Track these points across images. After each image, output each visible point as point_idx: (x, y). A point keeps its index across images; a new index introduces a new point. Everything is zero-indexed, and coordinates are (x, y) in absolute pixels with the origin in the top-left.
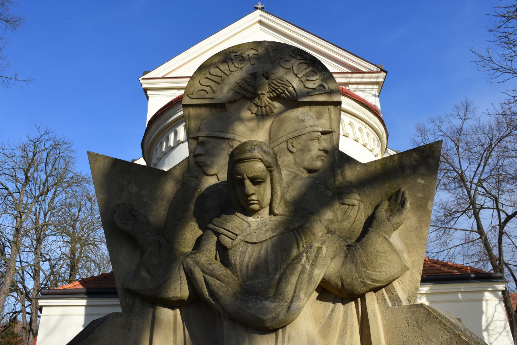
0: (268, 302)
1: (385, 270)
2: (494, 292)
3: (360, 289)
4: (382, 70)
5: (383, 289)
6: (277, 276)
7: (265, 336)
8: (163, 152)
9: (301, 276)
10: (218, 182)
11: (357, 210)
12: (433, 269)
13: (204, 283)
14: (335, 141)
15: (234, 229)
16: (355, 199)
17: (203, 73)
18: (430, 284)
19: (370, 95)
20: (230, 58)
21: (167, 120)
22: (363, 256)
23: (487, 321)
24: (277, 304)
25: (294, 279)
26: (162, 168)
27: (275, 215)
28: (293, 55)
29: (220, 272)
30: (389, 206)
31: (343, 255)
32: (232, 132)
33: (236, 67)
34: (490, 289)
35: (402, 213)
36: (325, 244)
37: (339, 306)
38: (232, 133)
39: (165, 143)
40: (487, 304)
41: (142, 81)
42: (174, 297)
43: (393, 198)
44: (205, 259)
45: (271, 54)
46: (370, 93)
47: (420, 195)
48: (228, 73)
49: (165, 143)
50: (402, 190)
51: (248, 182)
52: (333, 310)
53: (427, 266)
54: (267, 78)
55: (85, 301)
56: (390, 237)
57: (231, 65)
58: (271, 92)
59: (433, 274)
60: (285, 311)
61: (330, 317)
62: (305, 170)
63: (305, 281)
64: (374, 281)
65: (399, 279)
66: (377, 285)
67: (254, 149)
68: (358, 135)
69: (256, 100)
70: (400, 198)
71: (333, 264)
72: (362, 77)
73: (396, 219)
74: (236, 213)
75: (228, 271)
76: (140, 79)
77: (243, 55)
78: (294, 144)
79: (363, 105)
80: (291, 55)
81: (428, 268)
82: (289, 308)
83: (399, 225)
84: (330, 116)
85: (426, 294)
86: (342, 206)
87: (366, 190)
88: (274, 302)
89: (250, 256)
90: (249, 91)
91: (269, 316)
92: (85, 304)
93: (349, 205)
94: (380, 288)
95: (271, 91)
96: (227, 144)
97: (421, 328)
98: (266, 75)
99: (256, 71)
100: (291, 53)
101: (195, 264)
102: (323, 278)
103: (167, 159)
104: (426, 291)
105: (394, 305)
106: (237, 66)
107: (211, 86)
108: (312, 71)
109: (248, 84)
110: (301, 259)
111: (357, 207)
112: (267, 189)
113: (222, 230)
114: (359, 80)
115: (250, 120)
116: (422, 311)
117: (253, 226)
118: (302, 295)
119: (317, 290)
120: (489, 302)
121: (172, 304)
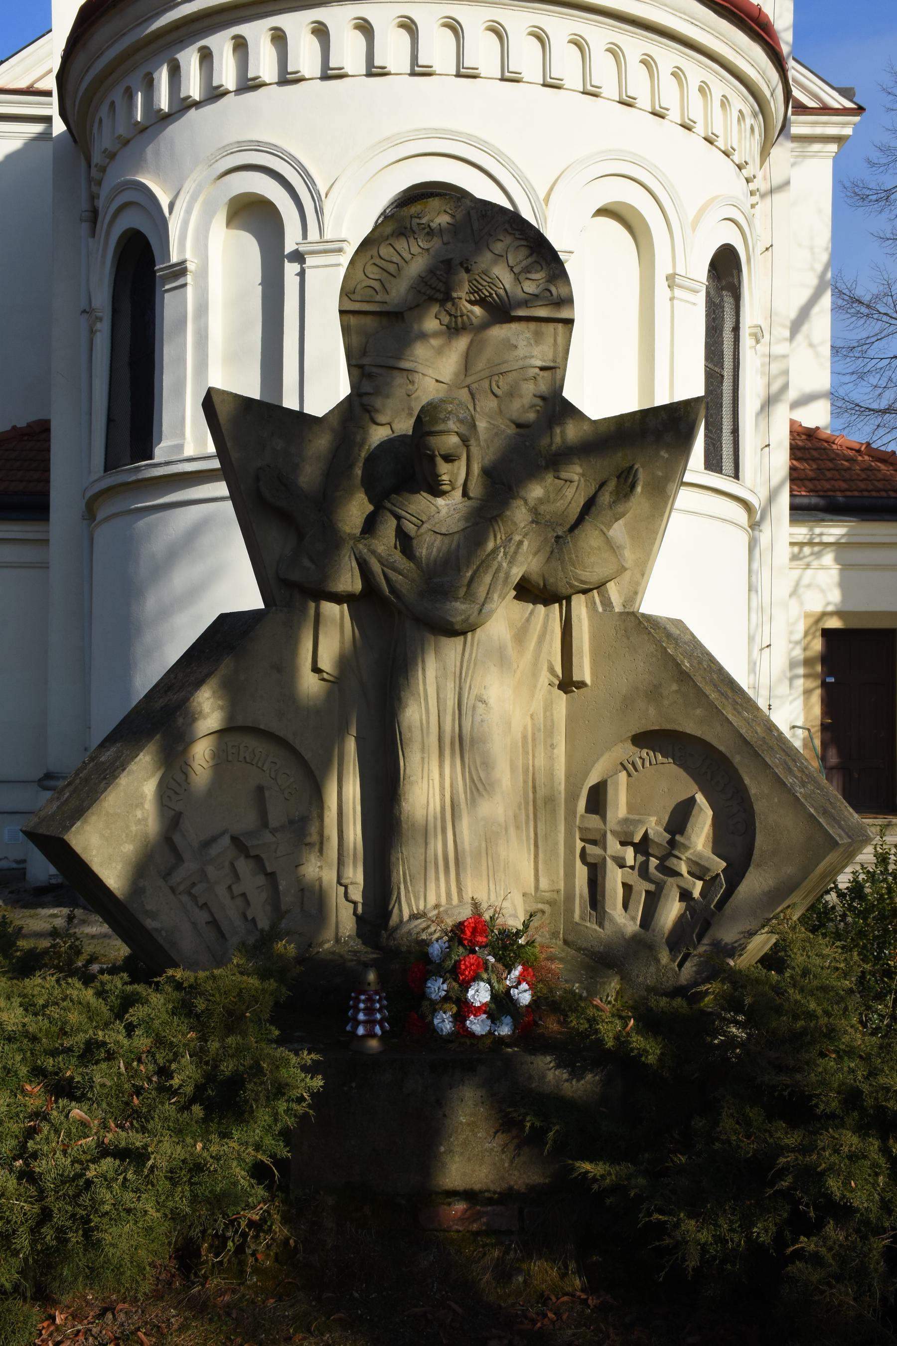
0: (458, 603)
1: (597, 570)
3: (564, 590)
5: (595, 592)
6: (469, 574)
7: (453, 639)
8: (139, 122)
9: (496, 575)
10: (393, 436)
11: (575, 488)
12: (873, 477)
13: (382, 577)
14: (558, 383)
15: (419, 514)
16: (575, 472)
17: (369, 254)
18: (852, 519)
20: (411, 228)
21: (145, 21)
22: (573, 552)
24: (468, 606)
25: (488, 579)
26: (136, 173)
27: (469, 498)
28: (510, 231)
29: (403, 566)
30: (617, 487)
31: (548, 549)
32: (412, 359)
33: (419, 246)
35: (629, 499)
36: (528, 537)
37: (541, 608)
38: (412, 361)
39: (140, 94)
42: (344, 591)
43: (624, 476)
44: (383, 547)
45: (476, 226)
47: (660, 474)
48: (407, 256)
49: (140, 94)
50: (636, 467)
51: (439, 460)
52: (532, 613)
53: (858, 467)
54: (468, 270)
56: (609, 530)
57: (411, 240)
58: (471, 293)
59: (869, 491)
60: (476, 613)
61: (528, 620)
62: (512, 424)
63: (500, 581)
64: (582, 582)
65: (616, 580)
66: (585, 586)
67: (449, 419)
68: (696, 111)
69: (449, 305)
70: (631, 477)
71: (535, 560)
73: (620, 508)
74: (422, 492)
75: (412, 565)
77: (431, 224)
78: (500, 384)
79: (721, 11)
80: (506, 230)
81: (859, 475)
82: (481, 610)
83: (623, 515)
84: (555, 340)
85: (836, 544)
86: (557, 481)
87: (592, 460)
88: (464, 603)
89: (439, 550)
90: (439, 291)
91: (459, 619)
93: (566, 481)
94: (591, 590)
95: (473, 291)
96: (405, 377)
97: (628, 638)
98: (465, 265)
99: (450, 256)
100: (507, 226)
101: (370, 553)
102: (523, 576)
103: (151, 146)
104: (838, 537)
105: (605, 610)
106: (422, 246)
107: (382, 280)
108: (536, 261)
109: (438, 279)
110: (498, 555)
111: (576, 484)
112: (462, 467)
113: (404, 513)
115: (435, 334)
116: (633, 621)
117: (444, 511)
118: (496, 597)
119: (515, 589)
121: (337, 598)
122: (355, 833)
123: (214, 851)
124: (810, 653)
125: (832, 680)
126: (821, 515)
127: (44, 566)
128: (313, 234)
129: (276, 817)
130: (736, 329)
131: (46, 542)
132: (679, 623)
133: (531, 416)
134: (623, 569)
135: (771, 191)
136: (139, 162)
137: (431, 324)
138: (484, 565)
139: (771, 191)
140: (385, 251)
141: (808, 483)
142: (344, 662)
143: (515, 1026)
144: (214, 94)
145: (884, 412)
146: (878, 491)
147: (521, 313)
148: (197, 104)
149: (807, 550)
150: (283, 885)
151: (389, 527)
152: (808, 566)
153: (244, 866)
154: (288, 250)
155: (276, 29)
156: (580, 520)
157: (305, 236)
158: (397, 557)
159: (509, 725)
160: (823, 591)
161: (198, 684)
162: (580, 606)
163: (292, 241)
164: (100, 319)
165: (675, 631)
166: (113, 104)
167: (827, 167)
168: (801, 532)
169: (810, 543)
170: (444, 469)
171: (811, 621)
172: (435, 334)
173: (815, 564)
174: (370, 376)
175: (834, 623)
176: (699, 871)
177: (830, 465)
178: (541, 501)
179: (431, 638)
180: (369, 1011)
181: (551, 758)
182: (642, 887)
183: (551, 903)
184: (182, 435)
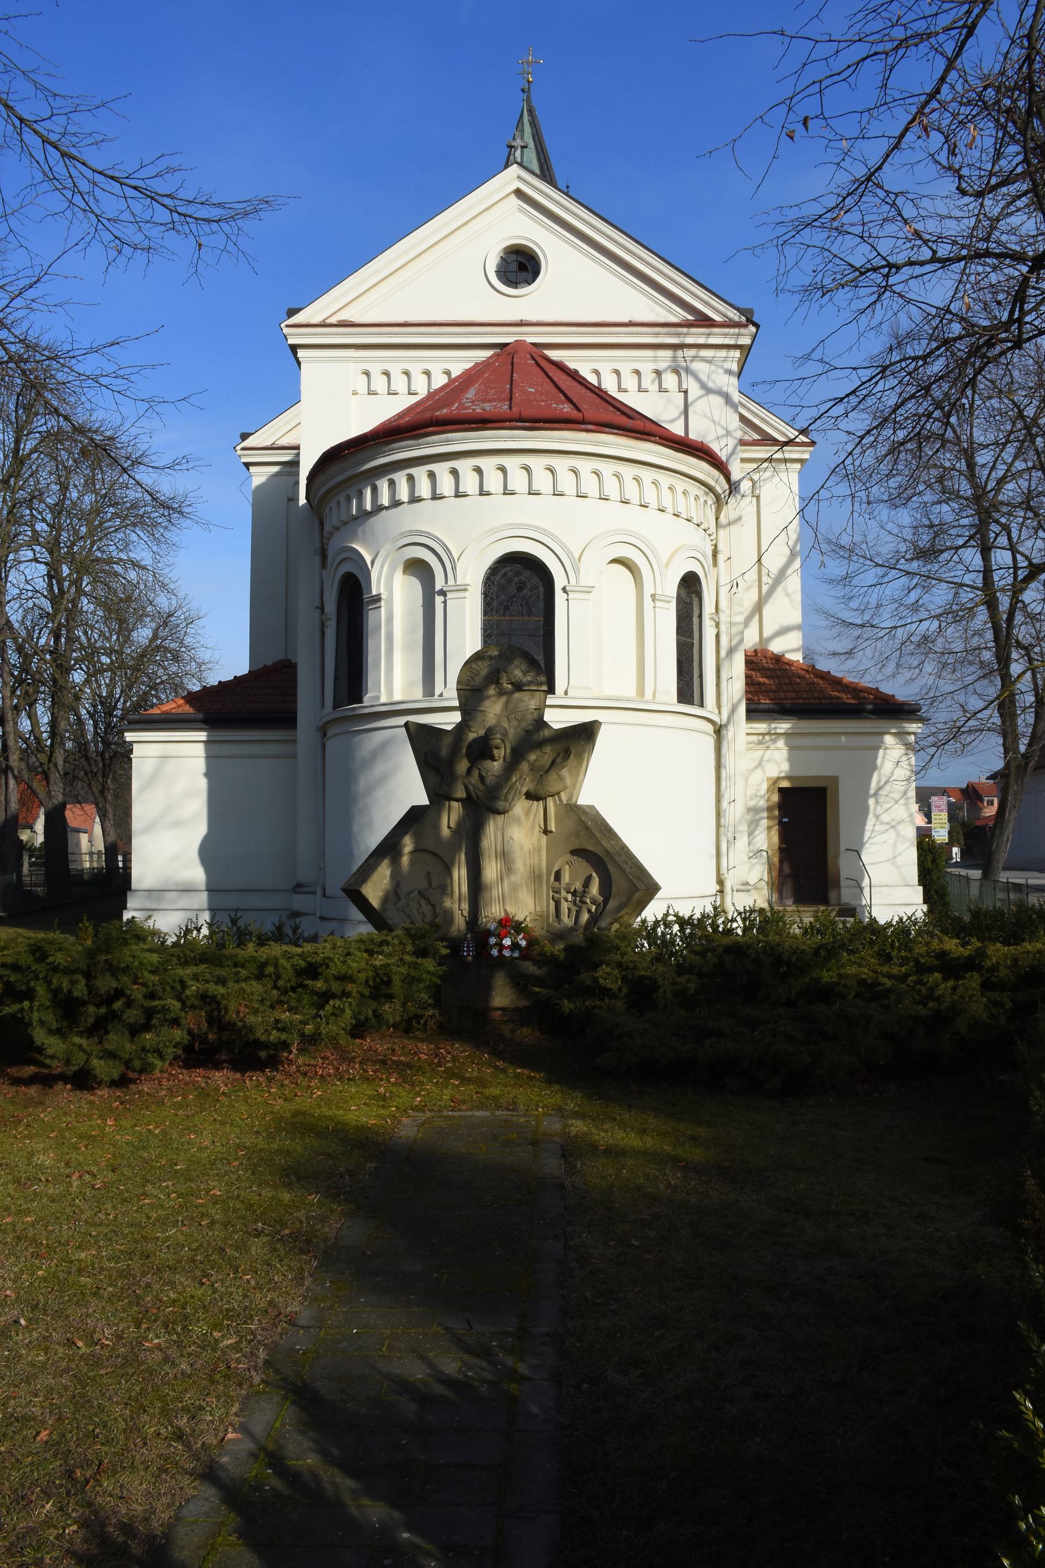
2: (901, 735)
3: (543, 796)
4: (750, 321)
16: (548, 749)
19: (721, 371)
23: (879, 782)
34: (893, 731)
40: (885, 754)
41: (286, 331)
46: (722, 367)
55: (205, 733)
68: (667, 501)
72: (709, 335)
76: (283, 325)
92: (204, 739)
114: (701, 341)
115: (493, 696)
120: (888, 751)
122: (465, 888)
123: (412, 896)
124: (770, 803)
125: (786, 820)
126: (776, 716)
127: (294, 756)
128: (451, 581)
129: (435, 884)
130: (700, 616)
131: (295, 741)
132: (592, 807)
133: (531, 728)
134: (566, 788)
135: (729, 524)
136: (354, 537)
137: (492, 691)
138: (512, 787)
139: (729, 524)
140: (474, 666)
141: (771, 694)
142: (459, 823)
143: (521, 952)
144: (396, 504)
145: (863, 626)
146: (815, 698)
147: (526, 688)
148: (386, 508)
149: (767, 738)
150: (438, 910)
151: (476, 773)
152: (768, 748)
153: (423, 902)
154: (438, 588)
155: (431, 471)
156: (550, 769)
157: (446, 582)
158: (479, 784)
159: (522, 848)
160: (778, 764)
161: (405, 834)
162: (550, 802)
163: (439, 584)
164: (330, 619)
165: (588, 810)
166: (338, 502)
167: (794, 478)
168: (762, 727)
169: (769, 734)
170: (496, 752)
171: (771, 782)
172: (493, 696)
173: (772, 746)
174: (469, 714)
175: (785, 784)
176: (594, 902)
177: (787, 681)
178: (535, 761)
179: (492, 816)
180: (468, 947)
181: (540, 860)
182: (574, 909)
183: (541, 916)
184: (379, 690)
